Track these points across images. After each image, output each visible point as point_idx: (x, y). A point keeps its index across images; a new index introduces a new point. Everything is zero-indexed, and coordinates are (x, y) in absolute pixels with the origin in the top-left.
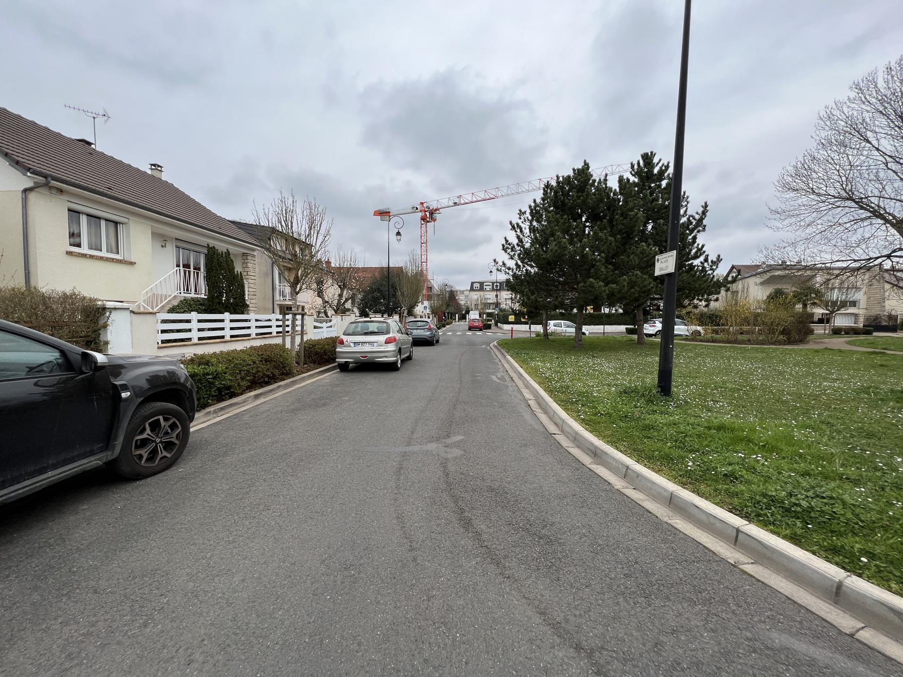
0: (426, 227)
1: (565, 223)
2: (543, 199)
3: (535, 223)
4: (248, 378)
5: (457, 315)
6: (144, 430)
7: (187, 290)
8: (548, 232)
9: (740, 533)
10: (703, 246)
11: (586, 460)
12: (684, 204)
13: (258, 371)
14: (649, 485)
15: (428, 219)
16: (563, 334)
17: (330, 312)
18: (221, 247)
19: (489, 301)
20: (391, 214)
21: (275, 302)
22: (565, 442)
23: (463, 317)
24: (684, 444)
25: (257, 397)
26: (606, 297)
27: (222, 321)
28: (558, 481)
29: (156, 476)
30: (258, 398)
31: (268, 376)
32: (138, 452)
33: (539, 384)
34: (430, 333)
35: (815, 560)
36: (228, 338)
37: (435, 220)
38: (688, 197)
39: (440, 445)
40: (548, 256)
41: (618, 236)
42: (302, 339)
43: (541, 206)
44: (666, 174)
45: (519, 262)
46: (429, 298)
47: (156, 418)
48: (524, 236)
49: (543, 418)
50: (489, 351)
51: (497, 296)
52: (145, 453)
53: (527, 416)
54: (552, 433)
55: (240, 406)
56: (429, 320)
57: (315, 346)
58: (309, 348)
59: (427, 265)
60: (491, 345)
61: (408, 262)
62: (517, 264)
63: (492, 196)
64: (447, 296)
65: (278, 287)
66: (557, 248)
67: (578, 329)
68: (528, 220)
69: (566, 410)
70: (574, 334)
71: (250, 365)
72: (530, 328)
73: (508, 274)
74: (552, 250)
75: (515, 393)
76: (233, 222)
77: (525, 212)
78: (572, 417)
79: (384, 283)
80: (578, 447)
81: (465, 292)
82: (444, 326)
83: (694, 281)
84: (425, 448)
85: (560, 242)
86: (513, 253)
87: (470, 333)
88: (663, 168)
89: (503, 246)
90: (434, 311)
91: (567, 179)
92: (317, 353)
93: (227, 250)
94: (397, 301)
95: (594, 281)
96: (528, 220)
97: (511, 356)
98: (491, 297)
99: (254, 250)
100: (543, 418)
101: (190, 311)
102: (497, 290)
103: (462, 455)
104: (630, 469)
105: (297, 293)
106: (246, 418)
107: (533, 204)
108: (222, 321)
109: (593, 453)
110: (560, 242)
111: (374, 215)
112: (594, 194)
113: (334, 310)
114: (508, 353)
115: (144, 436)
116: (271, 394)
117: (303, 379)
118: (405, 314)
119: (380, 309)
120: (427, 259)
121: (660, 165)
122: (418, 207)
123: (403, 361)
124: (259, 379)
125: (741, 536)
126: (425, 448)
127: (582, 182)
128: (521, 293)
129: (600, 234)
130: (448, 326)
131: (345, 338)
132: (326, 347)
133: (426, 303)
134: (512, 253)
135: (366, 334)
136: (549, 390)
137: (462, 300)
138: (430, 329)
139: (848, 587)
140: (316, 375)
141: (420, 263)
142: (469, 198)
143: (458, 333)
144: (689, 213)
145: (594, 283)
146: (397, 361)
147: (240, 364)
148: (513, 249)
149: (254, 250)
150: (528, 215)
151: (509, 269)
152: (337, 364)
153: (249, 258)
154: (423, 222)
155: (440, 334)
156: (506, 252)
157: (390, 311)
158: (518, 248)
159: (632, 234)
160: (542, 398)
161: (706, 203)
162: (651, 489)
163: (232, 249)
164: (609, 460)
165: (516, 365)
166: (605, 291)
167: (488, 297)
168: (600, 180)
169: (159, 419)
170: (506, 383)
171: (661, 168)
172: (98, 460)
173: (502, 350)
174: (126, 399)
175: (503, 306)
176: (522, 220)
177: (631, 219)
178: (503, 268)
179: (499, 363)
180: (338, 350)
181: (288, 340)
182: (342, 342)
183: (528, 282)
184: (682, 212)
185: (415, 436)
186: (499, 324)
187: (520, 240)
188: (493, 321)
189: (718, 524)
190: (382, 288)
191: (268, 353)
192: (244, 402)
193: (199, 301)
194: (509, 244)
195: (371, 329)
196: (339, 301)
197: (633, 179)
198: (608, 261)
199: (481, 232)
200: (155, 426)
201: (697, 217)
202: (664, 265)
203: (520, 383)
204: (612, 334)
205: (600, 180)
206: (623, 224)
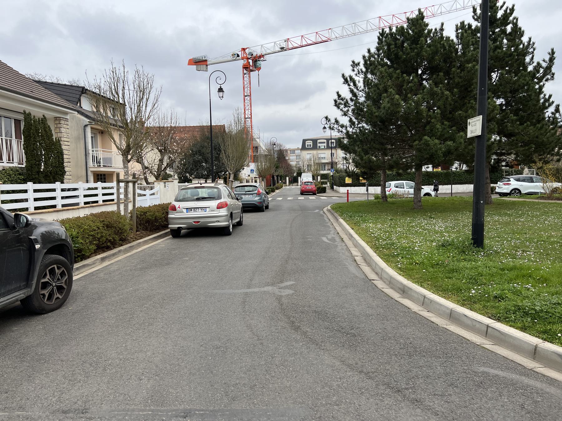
0: (250, 77)
1: (399, 78)
2: (378, 49)
3: (369, 76)
4: (95, 242)
5: (287, 178)
6: (46, 275)
7: (9, 160)
8: (381, 87)
9: (489, 328)
10: (550, 96)
11: (396, 296)
12: (531, 50)
13: (102, 236)
14: (438, 307)
15: (251, 68)
16: (406, 196)
17: (151, 179)
18: (37, 112)
19: (324, 161)
20: (208, 63)
21: (88, 169)
22: (380, 284)
23: (294, 180)
24: (476, 281)
25: (103, 259)
26: (442, 155)
27: (54, 190)
28: (368, 307)
29: (54, 312)
30: (104, 261)
31: (110, 241)
32: (42, 292)
33: (367, 243)
34: (258, 198)
35: (529, 337)
36: (59, 207)
37: (259, 69)
38: (534, 43)
39: (275, 288)
40: (382, 113)
41: (455, 90)
42: (134, 206)
43: (376, 56)
44: (511, 18)
45: (353, 119)
46: (255, 159)
47: (53, 266)
48: (358, 90)
49: (366, 269)
50: (322, 216)
51: (332, 154)
52: (46, 292)
53: (352, 268)
54: (372, 279)
55: (90, 267)
56: (257, 184)
57: (146, 213)
58: (141, 215)
59: (251, 121)
60: (325, 210)
61: (233, 121)
62: (351, 121)
63: (324, 39)
64: (276, 156)
65: (91, 152)
66: (389, 105)
67: (418, 190)
68: (362, 72)
69: (387, 261)
70: (413, 196)
71: (95, 230)
72: (367, 190)
73: (342, 132)
74: (384, 108)
75: (343, 251)
76: (39, 82)
77: (359, 64)
78: (390, 266)
79: (206, 144)
80: (392, 288)
81: (296, 152)
82: (273, 191)
83: (541, 134)
84: (262, 289)
85: (393, 99)
86: (346, 109)
87: (302, 198)
88: (508, 11)
89: (335, 101)
90: (262, 175)
91: (401, 30)
92: (148, 221)
93: (44, 116)
94: (221, 164)
95: (429, 139)
96: (362, 72)
97: (344, 220)
98: (325, 155)
99: (66, 113)
100: (366, 269)
101: (25, 181)
102: (331, 148)
103: (293, 294)
104: (426, 298)
105: (129, 161)
106: (102, 275)
107: (367, 55)
108: (54, 190)
109: (402, 290)
110: (393, 99)
111: (189, 64)
112: (429, 46)
113: (155, 176)
114: (341, 216)
115: (46, 280)
116: (114, 257)
117: (139, 245)
118: (231, 179)
119: (202, 174)
120: (251, 114)
121: (504, 8)
122: (240, 53)
123: (234, 226)
124: (103, 244)
125: (489, 330)
126: (262, 289)
127: (416, 33)
128: (355, 152)
129: (435, 89)
130: (277, 191)
131: (177, 204)
132: (157, 214)
133: (253, 166)
134: (346, 109)
135: (198, 199)
136: (376, 247)
137: (293, 160)
138: (259, 194)
139: (540, 347)
140: (150, 241)
141: (243, 120)
142: (297, 42)
143: (289, 199)
144: (536, 60)
145: (429, 141)
146: (229, 227)
147: (87, 229)
148: (346, 104)
149: (66, 113)
150: (362, 67)
151: (342, 126)
152: (169, 230)
153: (62, 122)
154: (245, 72)
155: (269, 199)
156: (338, 108)
157: (214, 175)
158: (352, 103)
159: (470, 87)
160: (368, 254)
161: (553, 50)
162: (439, 310)
163: (49, 115)
164: (413, 294)
165: (348, 227)
166: (441, 149)
167: (322, 156)
168: (436, 29)
169: (54, 267)
170: (336, 243)
171: (506, 11)
172: (22, 294)
173: (336, 214)
174: (38, 250)
175: (340, 166)
176: (355, 72)
177: (468, 72)
178: (336, 126)
179: (331, 226)
180: (170, 216)
181: (122, 207)
182: (174, 209)
183: (361, 141)
184: (528, 59)
185: (253, 282)
186: (335, 187)
187: (354, 95)
188: (328, 183)
189: (478, 325)
190: (204, 150)
191: (109, 220)
192: (94, 264)
193: (17, 171)
194: (342, 99)
195: (201, 195)
196: (160, 166)
197: (475, 24)
198: (444, 116)
199: (312, 80)
200: (52, 272)
201: (544, 65)
202: (474, 128)
203: (349, 243)
204: (460, 195)
205: (436, 29)
206: (460, 77)
